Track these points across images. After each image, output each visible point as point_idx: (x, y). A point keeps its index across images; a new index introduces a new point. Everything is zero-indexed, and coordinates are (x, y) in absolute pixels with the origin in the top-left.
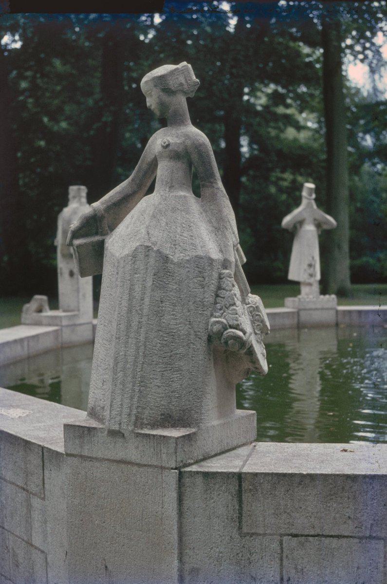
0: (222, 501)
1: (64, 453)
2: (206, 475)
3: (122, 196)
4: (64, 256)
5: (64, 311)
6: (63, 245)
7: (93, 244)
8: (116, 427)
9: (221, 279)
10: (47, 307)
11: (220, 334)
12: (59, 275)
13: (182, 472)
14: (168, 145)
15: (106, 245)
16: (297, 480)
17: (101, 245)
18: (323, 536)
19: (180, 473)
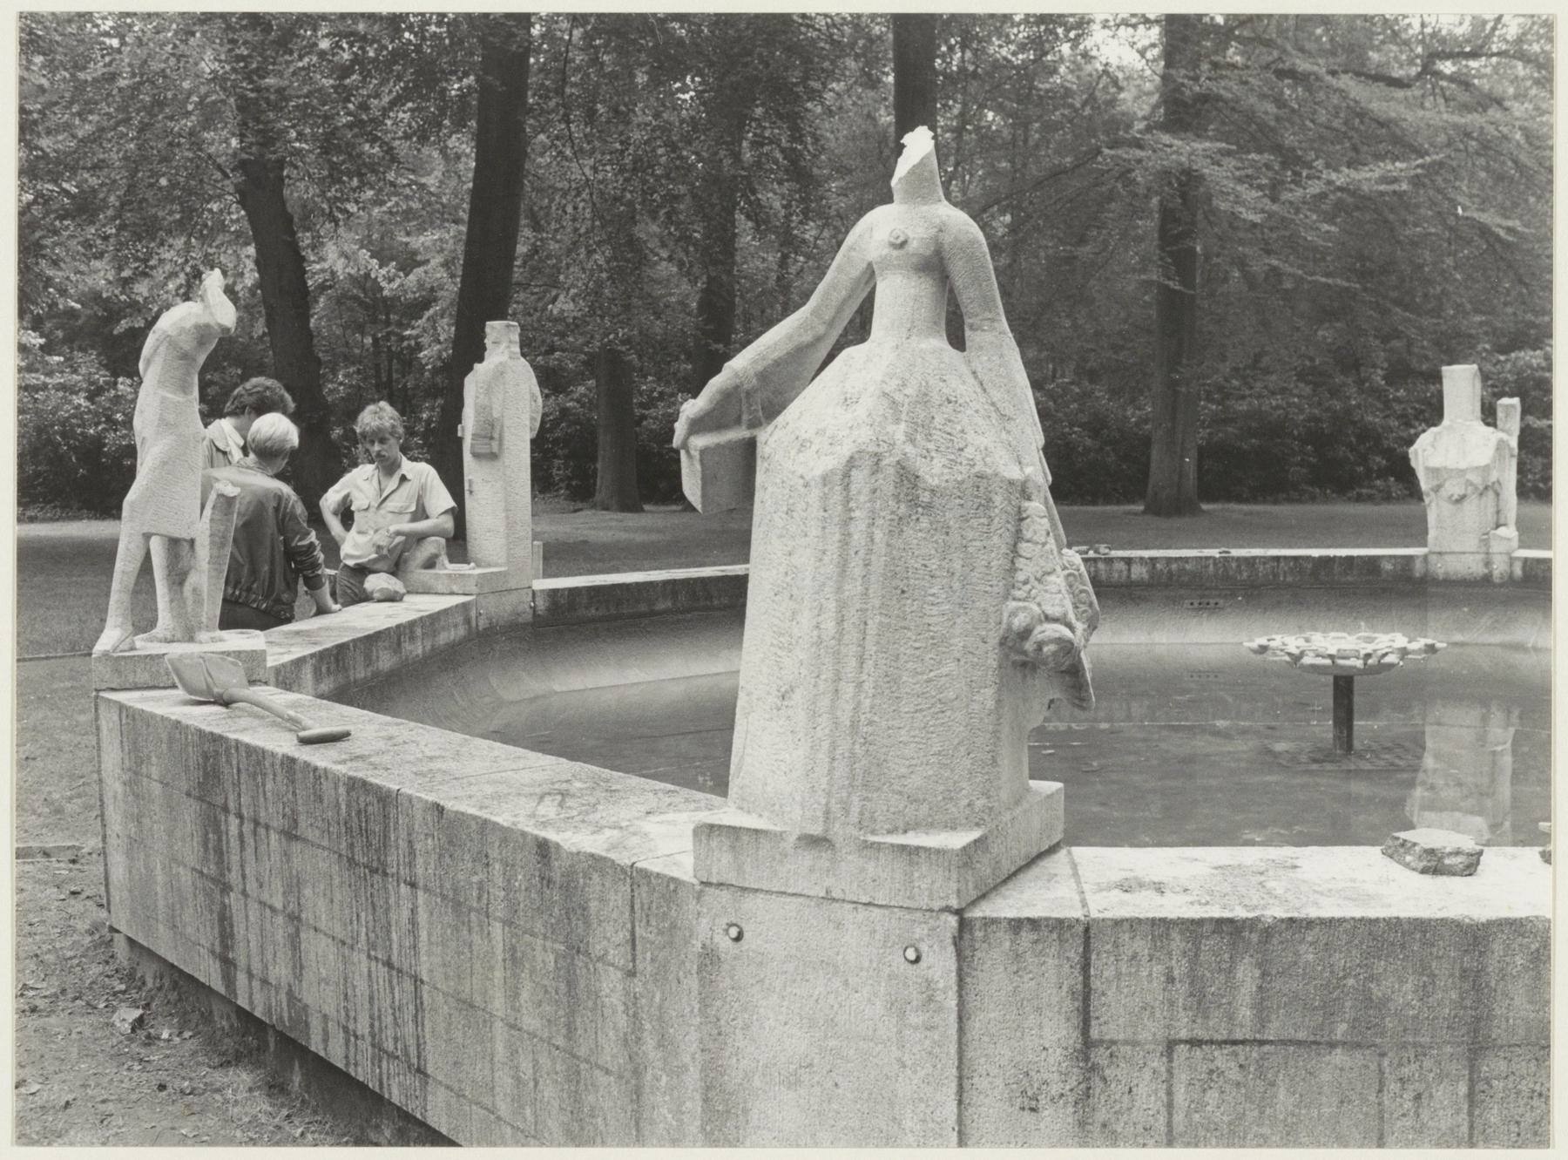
0: (1052, 975)
1: (695, 881)
2: (1016, 925)
3: (790, 346)
4: (476, 455)
5: (478, 566)
6: (475, 436)
7: (730, 446)
8: (816, 830)
9: (1022, 519)
10: (444, 559)
11: (1025, 633)
12: (467, 494)
13: (971, 920)
14: (903, 244)
15: (762, 450)
16: (1207, 928)
17: (750, 447)
18: (1234, 1043)
19: (964, 925)
